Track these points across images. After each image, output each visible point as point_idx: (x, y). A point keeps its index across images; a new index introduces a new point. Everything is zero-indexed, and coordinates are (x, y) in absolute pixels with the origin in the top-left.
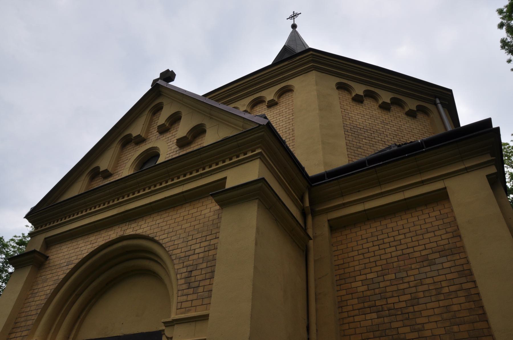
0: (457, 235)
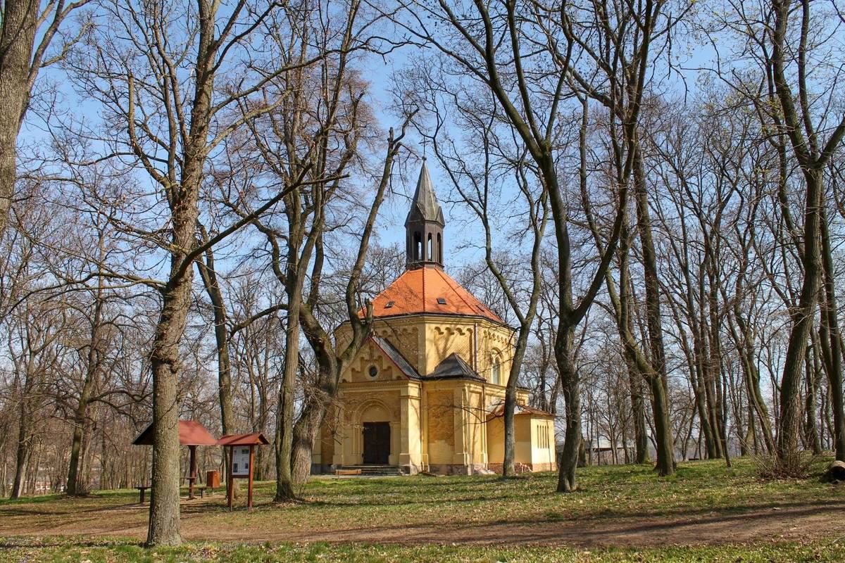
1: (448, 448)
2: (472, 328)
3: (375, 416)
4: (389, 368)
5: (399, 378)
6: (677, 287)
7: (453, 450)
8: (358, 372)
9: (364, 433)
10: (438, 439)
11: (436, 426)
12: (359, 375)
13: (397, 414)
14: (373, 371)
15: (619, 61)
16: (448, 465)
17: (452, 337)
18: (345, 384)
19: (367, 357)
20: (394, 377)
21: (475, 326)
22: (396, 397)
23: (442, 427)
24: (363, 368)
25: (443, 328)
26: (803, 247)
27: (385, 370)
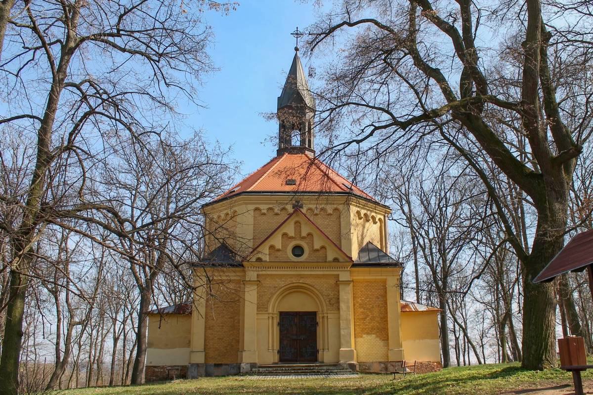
0: (386, 292)
1: (380, 343)
2: (382, 217)
3: (298, 304)
4: (323, 247)
5: (336, 260)
6: (13, 211)
7: (388, 345)
8: (278, 250)
9: (280, 324)
10: (368, 334)
11: (365, 318)
12: (279, 254)
13: (333, 302)
14: (298, 251)
15: (583, 137)
16: (380, 363)
17: (367, 224)
18: (258, 264)
19: (291, 233)
20: (330, 258)
21: (385, 216)
22: (332, 282)
23: (373, 319)
24: (284, 246)
25: (363, 212)
26: (452, 318)
27: (317, 250)
